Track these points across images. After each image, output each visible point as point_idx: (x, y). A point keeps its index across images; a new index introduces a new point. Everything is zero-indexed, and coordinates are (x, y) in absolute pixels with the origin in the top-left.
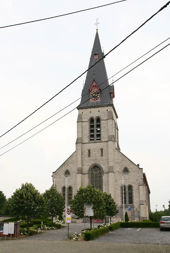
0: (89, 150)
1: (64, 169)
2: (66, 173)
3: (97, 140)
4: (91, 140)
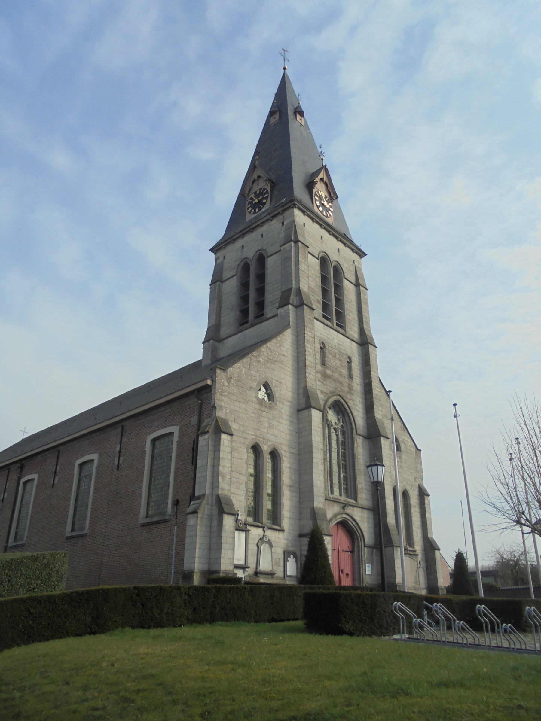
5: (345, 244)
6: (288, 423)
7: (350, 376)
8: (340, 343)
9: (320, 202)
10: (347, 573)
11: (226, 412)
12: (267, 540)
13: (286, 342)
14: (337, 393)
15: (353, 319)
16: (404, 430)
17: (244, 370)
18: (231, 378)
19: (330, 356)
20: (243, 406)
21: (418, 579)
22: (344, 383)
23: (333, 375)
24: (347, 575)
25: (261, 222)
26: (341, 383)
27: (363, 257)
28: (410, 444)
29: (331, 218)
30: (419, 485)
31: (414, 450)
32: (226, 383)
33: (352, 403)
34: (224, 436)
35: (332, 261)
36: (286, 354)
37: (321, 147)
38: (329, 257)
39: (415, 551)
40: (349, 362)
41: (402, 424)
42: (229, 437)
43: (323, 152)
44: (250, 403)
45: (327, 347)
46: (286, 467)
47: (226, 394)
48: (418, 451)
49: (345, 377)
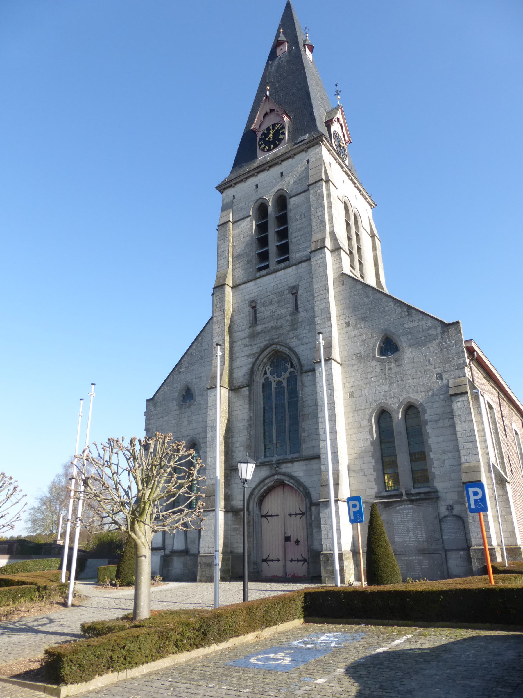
0: (254, 305)
1: (178, 386)
2: (184, 396)
3: (279, 262)
4: (260, 269)
10: (297, 540)
37: (337, 86)
43: (339, 91)
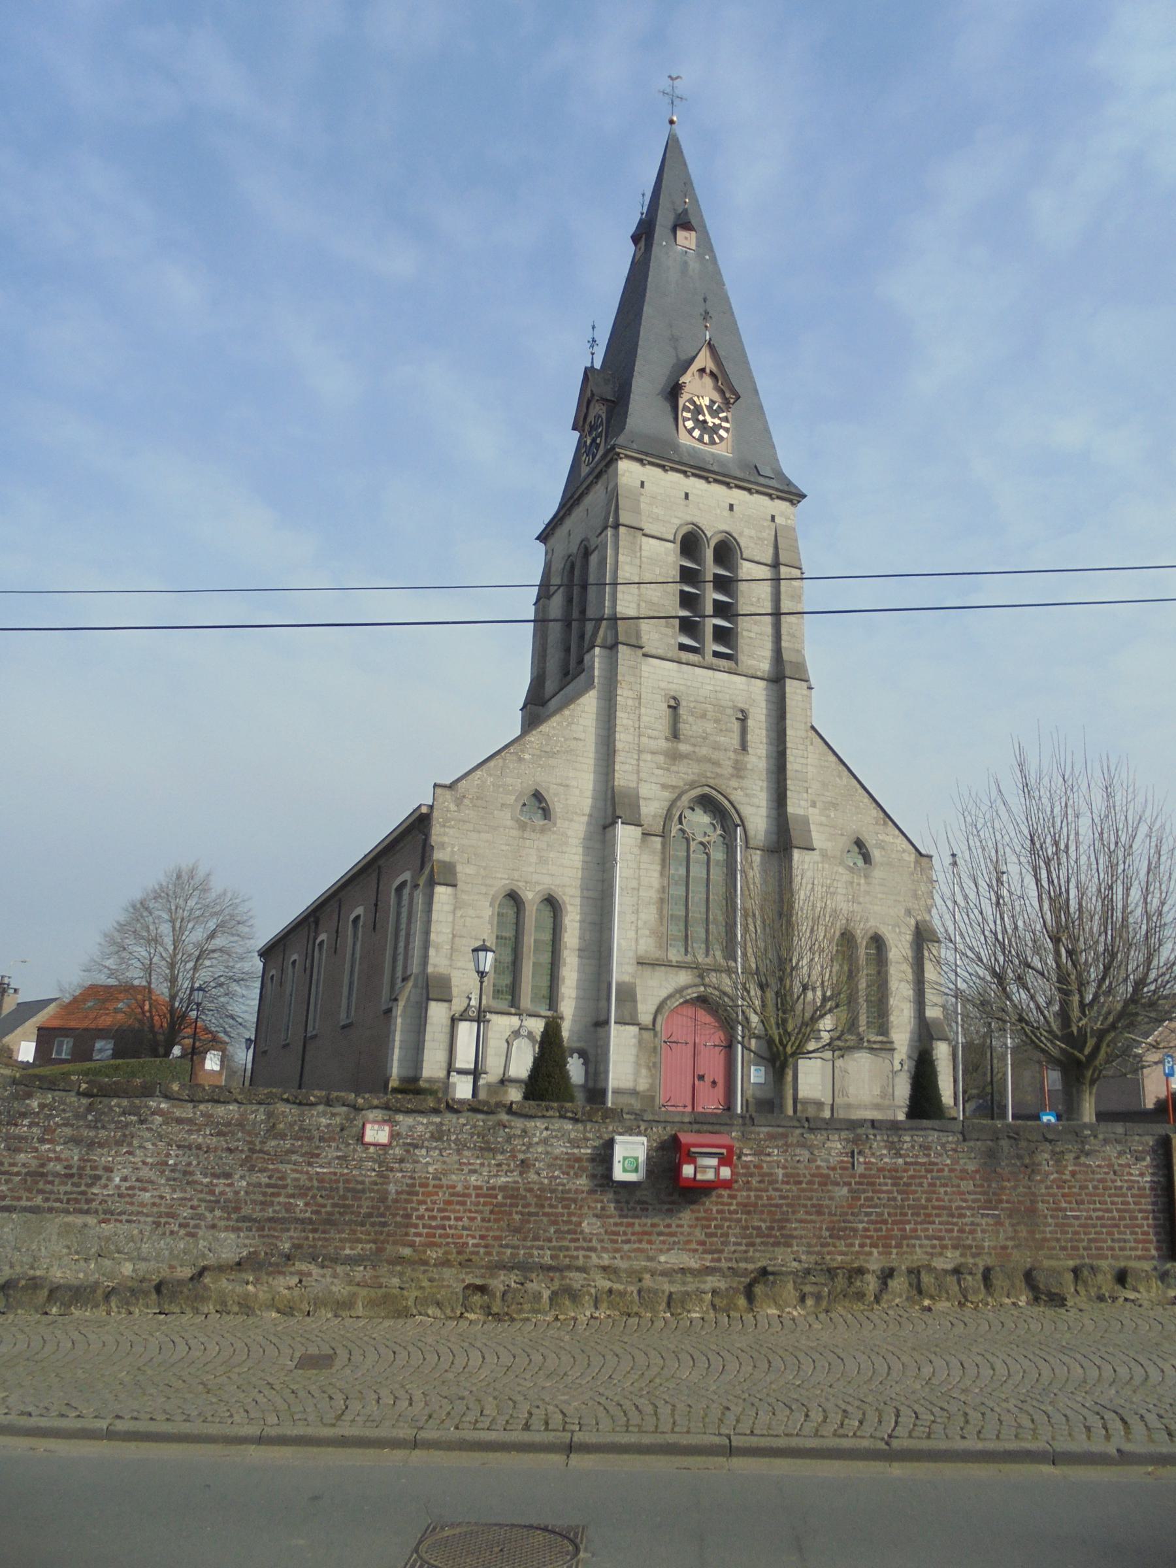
5: (749, 490)
6: (580, 850)
7: (744, 746)
8: (718, 689)
9: (696, 421)
11: (453, 852)
12: (526, 1033)
13: (584, 715)
14: (704, 781)
15: (761, 634)
16: (885, 824)
17: (490, 780)
18: (464, 797)
19: (691, 719)
20: (484, 836)
21: (890, 1090)
22: (721, 762)
23: (694, 752)
24: (714, 1083)
25: (584, 486)
26: (717, 764)
27: (799, 502)
28: (899, 848)
29: (724, 443)
30: (917, 924)
31: (911, 857)
32: (452, 807)
33: (741, 793)
34: (440, 890)
35: (709, 536)
36: (582, 736)
38: (702, 531)
39: (892, 1042)
40: (743, 720)
41: (880, 812)
42: (449, 890)
44: (502, 829)
45: (683, 703)
46: (573, 921)
47: (453, 823)
48: (925, 860)
49: (725, 750)
